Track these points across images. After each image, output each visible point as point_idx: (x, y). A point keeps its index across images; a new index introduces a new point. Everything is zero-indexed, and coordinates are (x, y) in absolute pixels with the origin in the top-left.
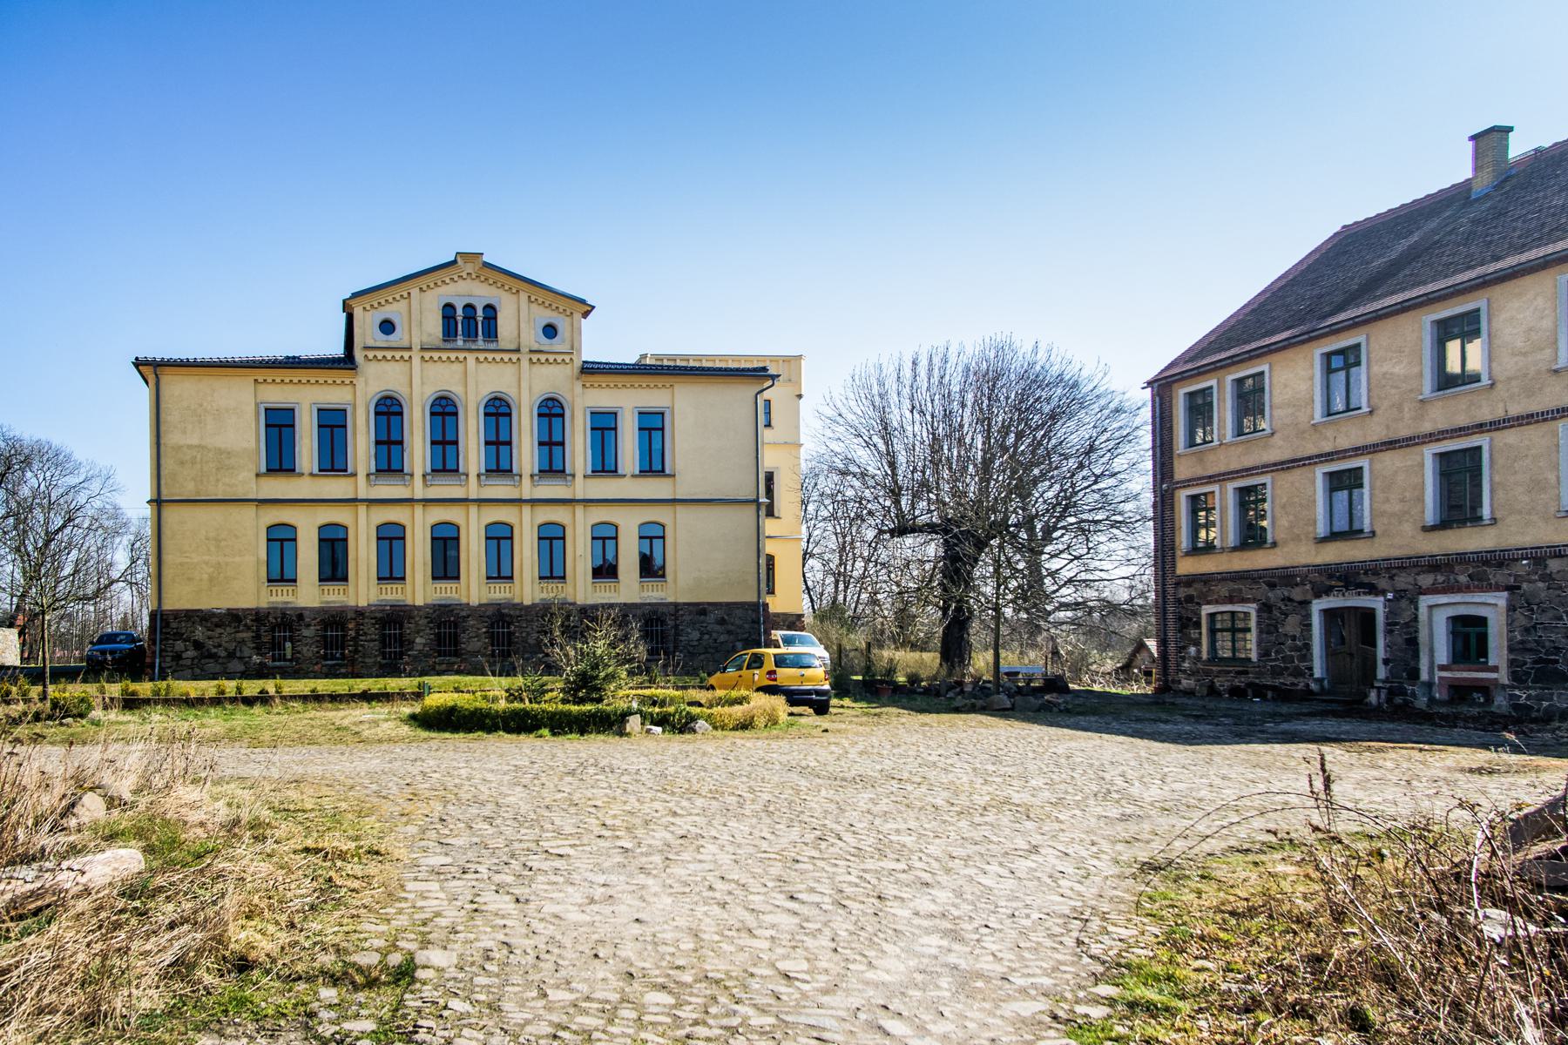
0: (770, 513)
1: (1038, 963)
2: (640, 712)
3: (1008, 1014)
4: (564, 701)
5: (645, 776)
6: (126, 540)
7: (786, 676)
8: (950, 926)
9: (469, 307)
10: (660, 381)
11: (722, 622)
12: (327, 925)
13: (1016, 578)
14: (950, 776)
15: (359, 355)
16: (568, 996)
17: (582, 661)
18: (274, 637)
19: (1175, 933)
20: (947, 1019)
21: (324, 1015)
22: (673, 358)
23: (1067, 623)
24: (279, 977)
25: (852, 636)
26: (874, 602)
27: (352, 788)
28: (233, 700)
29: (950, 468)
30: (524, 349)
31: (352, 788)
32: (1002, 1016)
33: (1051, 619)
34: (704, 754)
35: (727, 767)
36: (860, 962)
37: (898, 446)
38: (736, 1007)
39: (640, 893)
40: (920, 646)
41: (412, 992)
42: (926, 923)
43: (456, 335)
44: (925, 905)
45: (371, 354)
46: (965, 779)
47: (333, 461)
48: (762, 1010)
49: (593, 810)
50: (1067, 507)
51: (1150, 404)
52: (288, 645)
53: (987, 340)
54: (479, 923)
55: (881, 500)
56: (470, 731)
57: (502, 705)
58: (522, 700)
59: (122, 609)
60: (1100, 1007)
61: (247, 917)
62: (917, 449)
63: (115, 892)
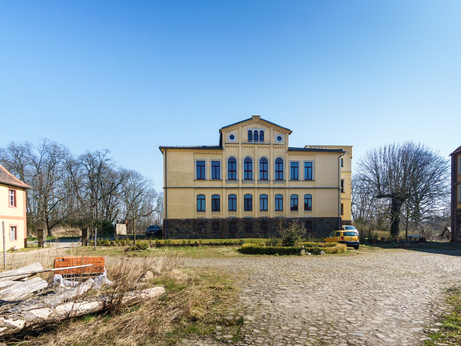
0: (342, 191)
1: (419, 317)
2: (304, 249)
3: (412, 331)
4: (283, 246)
5: (307, 267)
6: (156, 199)
7: (347, 238)
8: (395, 308)
9: (256, 131)
10: (311, 153)
11: (328, 223)
12: (218, 309)
13: (412, 210)
14: (394, 266)
15: (224, 145)
16: (287, 328)
17: (288, 234)
18: (199, 227)
19: (457, 308)
20: (395, 333)
21: (218, 333)
22: (315, 146)
23: (426, 223)
24: (204, 323)
25: (365, 227)
26: (372, 217)
27: (223, 270)
28: (187, 245)
29: (394, 179)
30: (272, 144)
31: (223, 270)
32: (410, 332)
33: (421, 221)
34: (323, 260)
35: (330, 264)
36: (370, 318)
37: (380, 172)
38: (335, 331)
39: (307, 300)
40: (385, 230)
41: (243, 327)
42: (388, 307)
43: (252, 140)
44: (387, 302)
45: (227, 145)
46: (398, 267)
47: (216, 176)
48: (343, 332)
49: (292, 276)
50: (427, 190)
51: (451, 160)
52: (203, 229)
53: (406, 142)
54: (261, 308)
55: (374, 188)
56: (255, 254)
57: (265, 247)
58: (270, 245)
59: (155, 219)
60: (437, 329)
61: (195, 306)
62: (385, 173)
63: (157, 299)
